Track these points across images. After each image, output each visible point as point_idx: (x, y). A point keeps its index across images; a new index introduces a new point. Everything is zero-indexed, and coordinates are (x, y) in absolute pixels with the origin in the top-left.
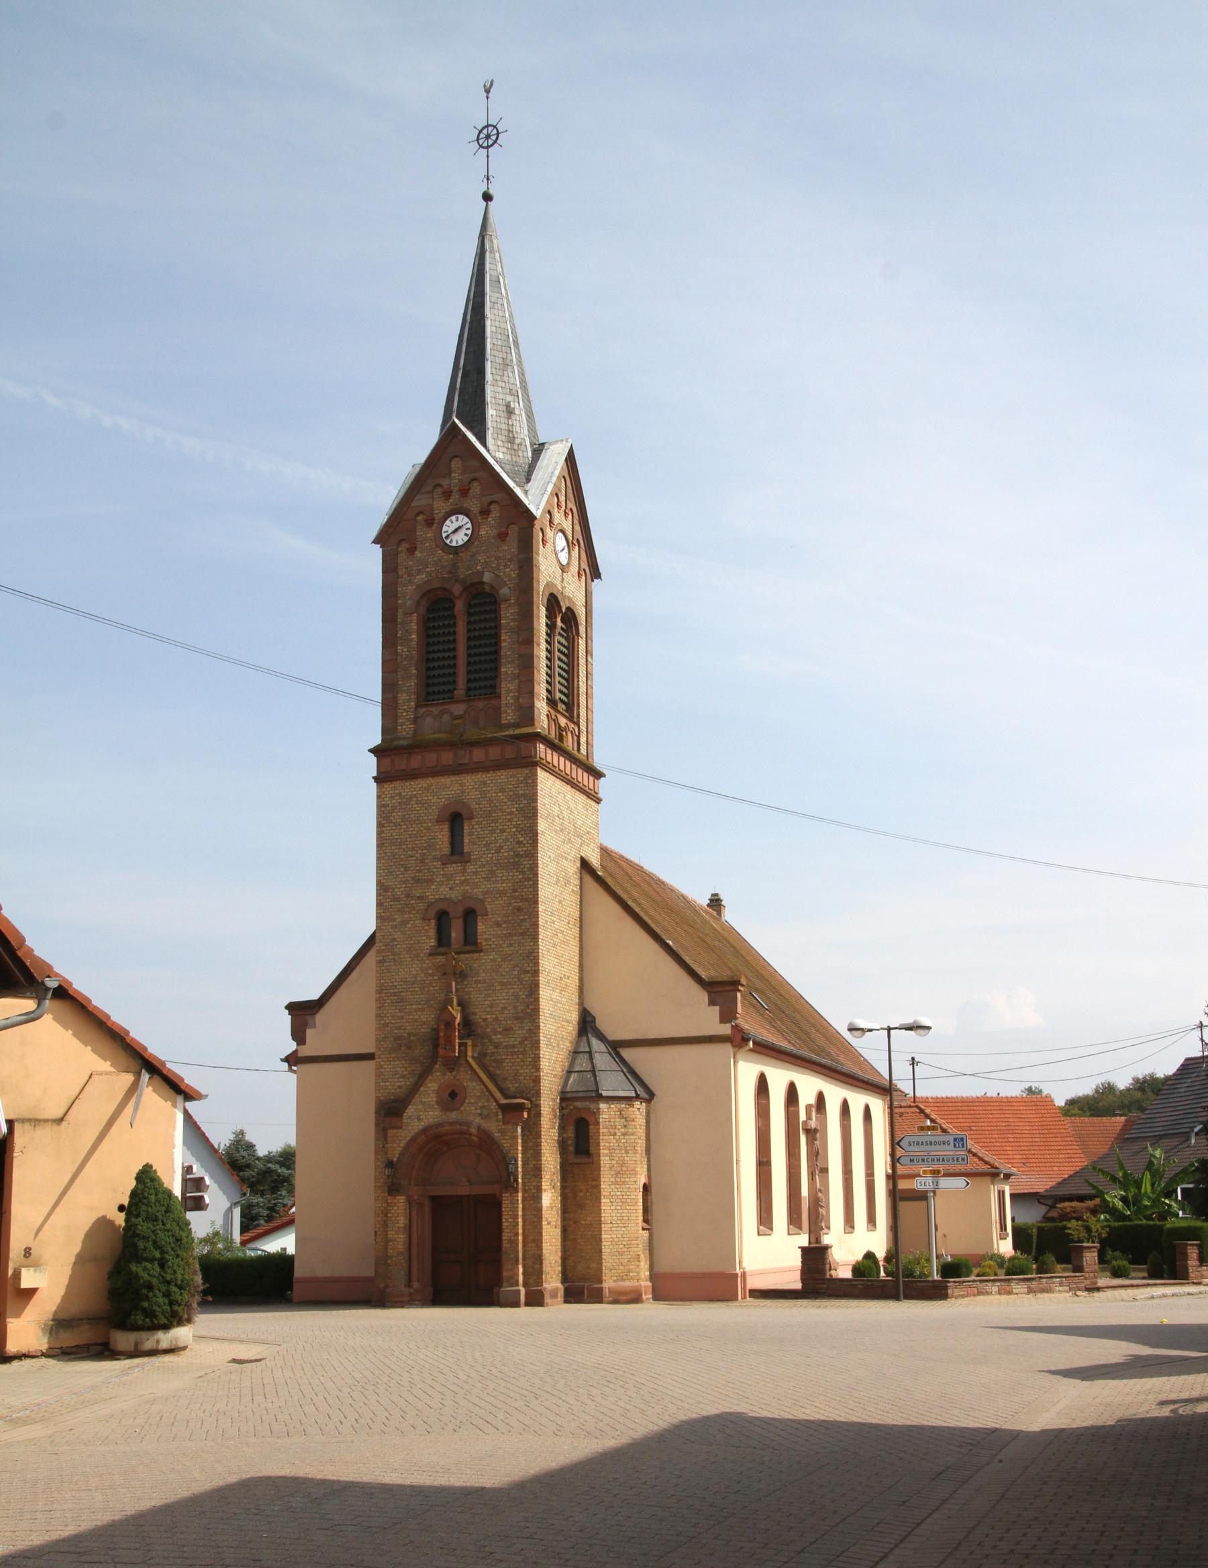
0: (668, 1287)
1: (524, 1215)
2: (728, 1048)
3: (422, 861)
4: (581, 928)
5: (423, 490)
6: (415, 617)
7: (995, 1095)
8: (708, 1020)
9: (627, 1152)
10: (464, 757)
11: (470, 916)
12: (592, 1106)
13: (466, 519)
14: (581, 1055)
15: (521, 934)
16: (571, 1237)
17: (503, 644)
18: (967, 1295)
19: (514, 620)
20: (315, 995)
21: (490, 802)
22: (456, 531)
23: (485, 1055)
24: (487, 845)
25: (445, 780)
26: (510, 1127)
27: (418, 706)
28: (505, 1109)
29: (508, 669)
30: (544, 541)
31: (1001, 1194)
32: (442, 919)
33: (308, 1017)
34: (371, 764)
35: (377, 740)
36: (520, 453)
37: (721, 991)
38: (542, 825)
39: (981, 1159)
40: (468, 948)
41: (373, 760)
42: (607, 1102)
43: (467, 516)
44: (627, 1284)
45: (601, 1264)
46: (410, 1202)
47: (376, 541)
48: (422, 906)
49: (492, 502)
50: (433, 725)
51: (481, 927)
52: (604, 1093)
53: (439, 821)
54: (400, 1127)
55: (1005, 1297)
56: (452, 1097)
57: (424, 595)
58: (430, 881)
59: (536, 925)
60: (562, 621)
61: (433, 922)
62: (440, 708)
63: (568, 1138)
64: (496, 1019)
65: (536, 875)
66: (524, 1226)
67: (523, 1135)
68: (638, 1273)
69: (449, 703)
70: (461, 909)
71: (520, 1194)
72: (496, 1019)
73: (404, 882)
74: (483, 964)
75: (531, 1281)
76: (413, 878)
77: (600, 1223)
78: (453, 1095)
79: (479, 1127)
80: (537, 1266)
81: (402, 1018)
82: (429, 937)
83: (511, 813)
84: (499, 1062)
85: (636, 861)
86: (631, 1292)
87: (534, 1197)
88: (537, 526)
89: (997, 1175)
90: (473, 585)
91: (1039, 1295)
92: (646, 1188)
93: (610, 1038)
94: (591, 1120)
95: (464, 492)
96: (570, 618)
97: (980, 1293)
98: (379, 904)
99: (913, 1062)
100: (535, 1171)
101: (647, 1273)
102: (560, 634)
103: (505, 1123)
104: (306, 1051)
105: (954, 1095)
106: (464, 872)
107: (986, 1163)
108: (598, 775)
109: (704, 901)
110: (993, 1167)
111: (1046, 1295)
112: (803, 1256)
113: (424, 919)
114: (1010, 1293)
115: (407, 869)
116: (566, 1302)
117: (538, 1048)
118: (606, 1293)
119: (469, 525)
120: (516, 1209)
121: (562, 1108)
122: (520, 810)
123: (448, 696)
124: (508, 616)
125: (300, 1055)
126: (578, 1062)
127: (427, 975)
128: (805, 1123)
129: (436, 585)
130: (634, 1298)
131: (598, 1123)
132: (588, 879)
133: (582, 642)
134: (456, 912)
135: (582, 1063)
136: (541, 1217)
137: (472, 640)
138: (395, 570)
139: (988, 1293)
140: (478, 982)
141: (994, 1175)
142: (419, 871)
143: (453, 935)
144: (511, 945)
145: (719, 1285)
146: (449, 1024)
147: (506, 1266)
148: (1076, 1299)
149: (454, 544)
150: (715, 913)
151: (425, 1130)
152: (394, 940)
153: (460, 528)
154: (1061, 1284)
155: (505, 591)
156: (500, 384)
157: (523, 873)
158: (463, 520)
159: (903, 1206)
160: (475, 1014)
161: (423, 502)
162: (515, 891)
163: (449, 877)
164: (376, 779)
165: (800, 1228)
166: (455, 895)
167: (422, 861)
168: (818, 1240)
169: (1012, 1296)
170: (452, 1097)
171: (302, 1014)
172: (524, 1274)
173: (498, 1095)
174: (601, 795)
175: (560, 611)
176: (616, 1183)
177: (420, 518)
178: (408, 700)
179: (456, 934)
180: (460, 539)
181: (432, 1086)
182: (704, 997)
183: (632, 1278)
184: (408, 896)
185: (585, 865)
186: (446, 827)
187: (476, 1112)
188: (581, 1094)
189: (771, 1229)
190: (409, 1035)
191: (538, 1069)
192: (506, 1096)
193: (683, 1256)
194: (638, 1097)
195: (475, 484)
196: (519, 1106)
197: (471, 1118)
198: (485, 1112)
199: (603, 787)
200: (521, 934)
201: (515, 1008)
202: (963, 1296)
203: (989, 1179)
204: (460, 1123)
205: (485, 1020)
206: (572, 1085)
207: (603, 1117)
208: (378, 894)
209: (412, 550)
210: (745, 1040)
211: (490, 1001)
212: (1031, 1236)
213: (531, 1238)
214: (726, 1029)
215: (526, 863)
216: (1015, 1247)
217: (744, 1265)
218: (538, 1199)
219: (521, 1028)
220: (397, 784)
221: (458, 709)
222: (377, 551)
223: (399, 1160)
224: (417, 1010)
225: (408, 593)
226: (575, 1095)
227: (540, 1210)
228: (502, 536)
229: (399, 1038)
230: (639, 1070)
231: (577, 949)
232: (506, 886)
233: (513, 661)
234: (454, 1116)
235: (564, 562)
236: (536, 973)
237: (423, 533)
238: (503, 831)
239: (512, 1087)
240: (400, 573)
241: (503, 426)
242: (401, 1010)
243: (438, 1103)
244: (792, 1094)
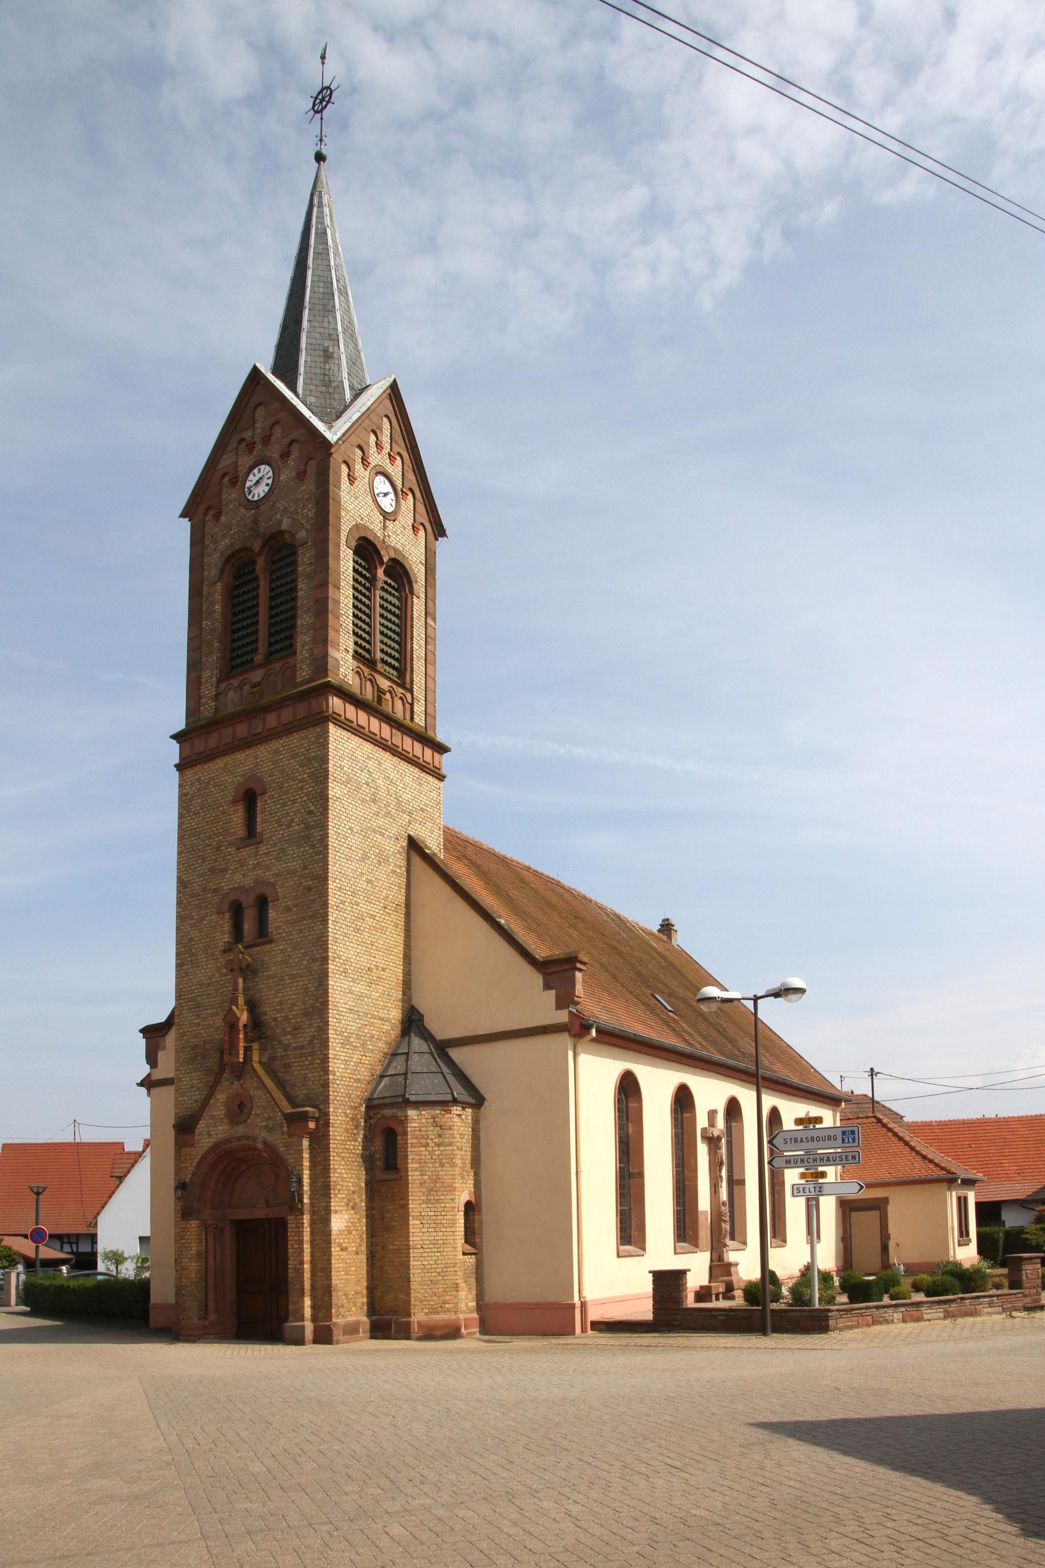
0: (498, 1320)
1: (312, 1242)
2: (565, 1039)
3: (218, 849)
4: (408, 915)
5: (229, 449)
6: (219, 586)
7: (994, 1116)
8: (543, 1007)
9: (442, 1165)
10: (258, 726)
11: (262, 903)
12: (400, 1113)
13: (268, 468)
14: (398, 1058)
15: (311, 917)
16: (378, 1264)
17: (300, 594)
18: (858, 1326)
19: (310, 564)
20: (162, 1018)
21: (282, 771)
22: (258, 482)
23: (273, 1059)
24: (279, 821)
25: (240, 756)
26: (295, 1140)
27: (220, 681)
28: (290, 1118)
29: (304, 619)
30: (352, 479)
31: (962, 1202)
32: (237, 911)
33: (160, 1039)
34: (173, 752)
35: (180, 725)
36: (336, 396)
37: (557, 972)
38: (335, 790)
39: (937, 1165)
40: (261, 940)
41: (175, 746)
42: (417, 1109)
43: (269, 465)
44: (441, 1317)
45: (408, 1294)
46: (206, 1227)
47: (183, 515)
48: (216, 899)
49: (276, 423)
50: (233, 701)
51: (272, 914)
52: (413, 1098)
53: (234, 802)
54: (192, 1145)
55: (911, 1325)
56: (239, 1110)
57: (227, 560)
58: (225, 870)
59: (325, 905)
60: (386, 573)
61: (227, 915)
62: (240, 678)
63: (376, 1152)
64: (286, 1018)
65: (326, 847)
66: (312, 1253)
67: (311, 1148)
68: (456, 1304)
69: (247, 671)
70: (252, 897)
71: (306, 1219)
72: (286, 1018)
73: (202, 875)
74: (275, 957)
75: (321, 1315)
76: (210, 869)
77: (408, 1247)
78: (241, 1105)
79: (265, 1142)
80: (326, 1298)
81: (198, 1025)
82: (223, 933)
83: (303, 780)
84: (288, 1066)
85: (553, 875)
86: (445, 1326)
87: (321, 1221)
88: (337, 457)
89: (954, 1180)
90: (273, 536)
91: (960, 1320)
92: (470, 1208)
93: (438, 1038)
94: (399, 1129)
95: (267, 439)
96: (398, 571)
97: (875, 1322)
98: (179, 903)
99: (872, 1073)
100: (323, 1189)
101: (473, 1304)
102: (383, 589)
103: (290, 1136)
104: (159, 1074)
105: (956, 1118)
106: (257, 854)
107: (943, 1168)
108: (441, 749)
109: (655, 927)
110: (949, 1172)
111: (970, 1320)
112: (655, 1282)
113: (219, 913)
114: (919, 1319)
115: (204, 860)
116: (372, 1337)
117: (327, 1048)
118: (415, 1328)
119: (271, 474)
120: (301, 1234)
121: (368, 1118)
122: (311, 775)
123: (248, 665)
124: (305, 560)
125: (153, 1078)
126: (394, 1065)
127: (222, 975)
128: (704, 1130)
129: (238, 546)
130: (452, 1333)
131: (406, 1133)
132: (417, 860)
133: (418, 606)
134: (248, 900)
135: (398, 1066)
136: (329, 1243)
137: (281, 602)
138: (202, 540)
139: (887, 1322)
140: (270, 977)
141: (950, 1181)
142: (215, 861)
143: (246, 927)
144: (301, 931)
145: (550, 1318)
146: (232, 1026)
147: (292, 1299)
148: (1009, 1321)
149: (256, 498)
150: (665, 938)
151: (214, 1147)
152: (192, 939)
153: (261, 478)
154: (991, 1305)
155: (302, 534)
156: (318, 330)
157: (313, 846)
158: (265, 469)
159: (856, 1216)
160: (265, 1014)
161: (228, 462)
162: (305, 868)
163: (242, 863)
164: (178, 767)
165: (696, 1246)
166: (248, 882)
167: (218, 849)
168: (720, 1258)
169: (923, 1323)
170: (239, 1110)
171: (153, 1034)
172: (313, 1307)
173: (284, 1103)
174: (444, 772)
175: (382, 563)
176: (428, 1201)
177: (226, 480)
178: (209, 675)
179: (249, 926)
180: (261, 491)
181: (221, 1097)
182: (538, 980)
183: (448, 1310)
184: (204, 889)
185: (414, 845)
186: (240, 808)
187: (262, 1128)
188: (388, 1101)
189: (644, 1249)
190: (205, 1043)
191: (326, 1071)
192: (294, 1104)
193: (512, 1284)
194: (455, 1101)
195: (277, 428)
196: (308, 1115)
197: (257, 1132)
198: (271, 1124)
199: (445, 762)
200: (311, 917)
201: (304, 1002)
202: (851, 1328)
203: (945, 1184)
204: (247, 1138)
205: (275, 1019)
206: (381, 1091)
207: (412, 1126)
208: (179, 892)
209: (217, 516)
210: (586, 1028)
211: (280, 1000)
212: (997, 1241)
213: (320, 1266)
214: (562, 1017)
215: (317, 834)
216: (981, 1251)
217: (585, 1293)
218: (326, 1221)
219: (310, 1026)
220: (196, 769)
221: (256, 676)
222: (186, 524)
223: (191, 1181)
224: (212, 1015)
225: (214, 560)
226: (381, 1101)
227: (329, 1234)
228: (301, 476)
229: (195, 1047)
230: (469, 1072)
231: (401, 940)
232: (296, 865)
233: (309, 610)
234: (241, 1130)
235: (389, 509)
236: (325, 960)
237: (229, 495)
238: (294, 802)
239: (300, 1093)
240: (207, 543)
241: (318, 371)
242: (198, 1016)
243: (226, 1116)
244: (683, 1099)
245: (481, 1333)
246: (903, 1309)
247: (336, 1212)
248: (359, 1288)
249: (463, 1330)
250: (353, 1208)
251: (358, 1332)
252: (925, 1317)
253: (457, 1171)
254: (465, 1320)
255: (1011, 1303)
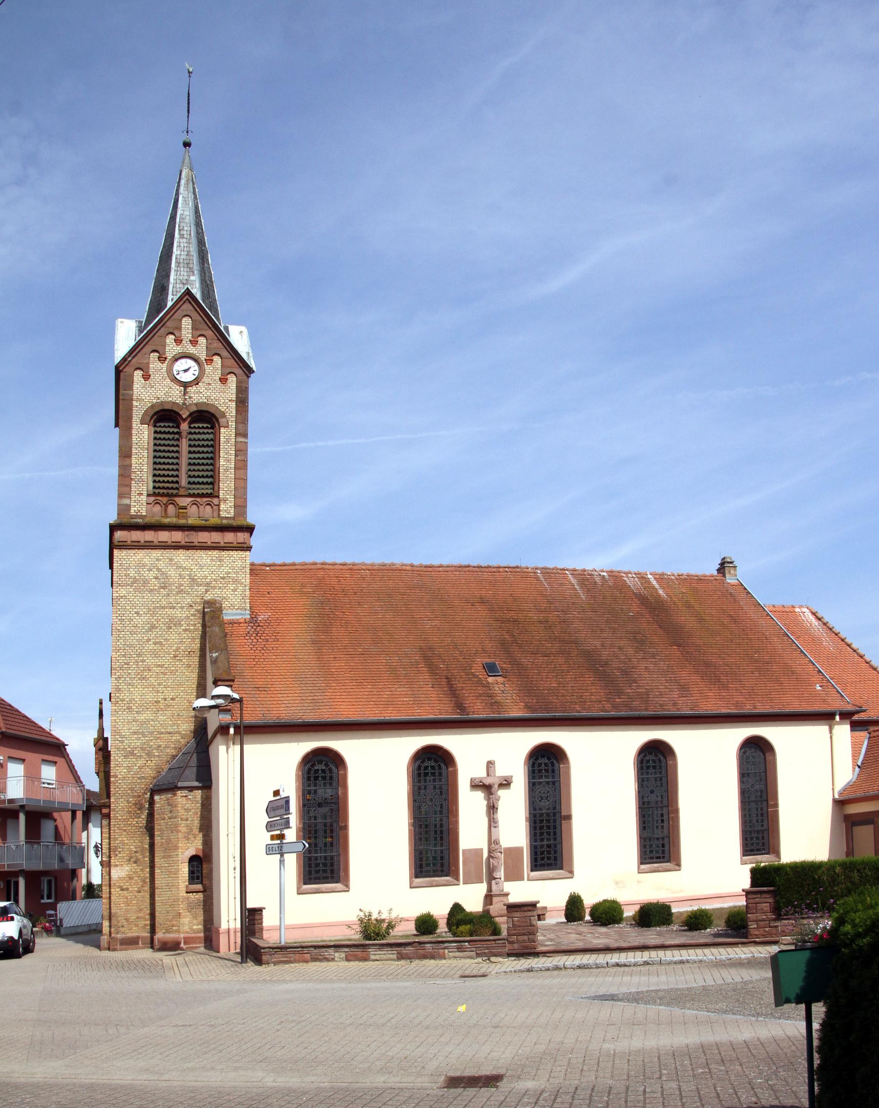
114: (366, 959)
231: (195, 676)
245: (205, 947)
246: (346, 950)
247: (116, 866)
248: (141, 915)
249: (182, 945)
250: (135, 862)
251: (138, 944)
252: (373, 957)
253: (180, 835)
254: (184, 938)
255: (487, 948)
